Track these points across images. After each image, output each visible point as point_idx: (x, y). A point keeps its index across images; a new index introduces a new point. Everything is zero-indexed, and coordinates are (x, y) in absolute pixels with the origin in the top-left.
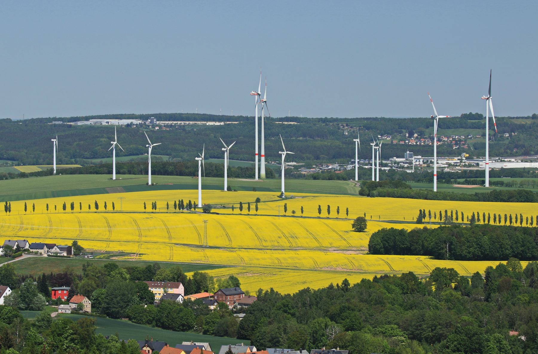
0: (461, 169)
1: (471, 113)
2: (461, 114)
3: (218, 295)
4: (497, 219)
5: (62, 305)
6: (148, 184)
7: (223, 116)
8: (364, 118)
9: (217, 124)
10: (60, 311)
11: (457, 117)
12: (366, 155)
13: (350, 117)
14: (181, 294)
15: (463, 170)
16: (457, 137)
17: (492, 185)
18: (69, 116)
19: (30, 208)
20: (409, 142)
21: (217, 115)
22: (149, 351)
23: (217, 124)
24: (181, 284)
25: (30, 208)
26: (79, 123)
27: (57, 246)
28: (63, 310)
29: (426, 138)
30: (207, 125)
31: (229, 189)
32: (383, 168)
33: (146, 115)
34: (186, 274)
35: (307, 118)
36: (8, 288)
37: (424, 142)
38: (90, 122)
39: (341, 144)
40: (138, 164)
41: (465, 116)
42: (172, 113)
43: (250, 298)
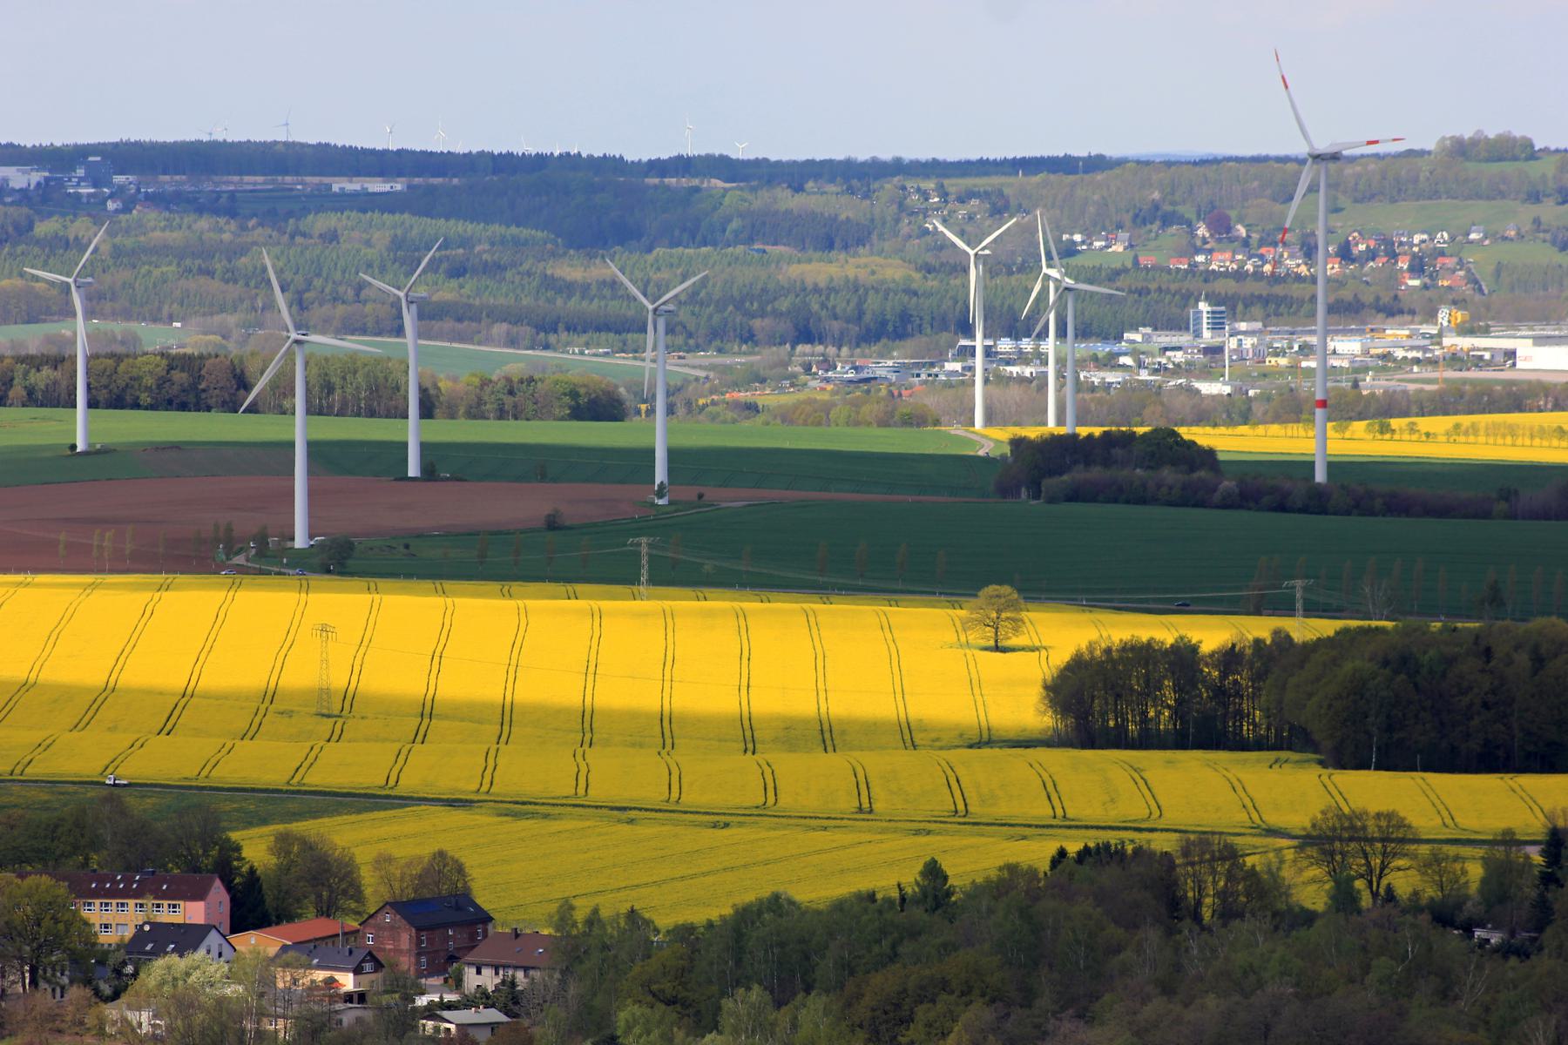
0: (1436, 375)
1: (225, 141)
3: (379, 928)
4: (522, 611)
6: (74, 447)
7: (400, 152)
8: (1014, 159)
14: (215, 927)
15: (1446, 380)
16: (1417, 239)
20: (1208, 262)
21: (379, 147)
24: (218, 883)
30: (335, 194)
33: (151, 142)
34: (235, 836)
35: (766, 160)
37: (1277, 263)
39: (917, 276)
40: (35, 362)
41: (1461, 150)
42: (46, 142)
43: (519, 939)
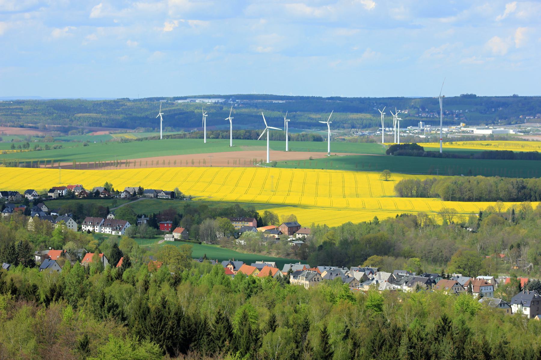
2: (513, 94)
5: (167, 235)
9: (281, 102)
10: (166, 239)
11: (458, 97)
12: (389, 125)
13: (378, 97)
17: (145, 117)
18: (172, 96)
19: (439, 279)
22: (231, 268)
23: (281, 102)
25: (439, 279)
26: (274, 101)
27: (164, 191)
28: (168, 238)
29: (434, 112)
31: (290, 150)
32: (402, 135)
34: (258, 211)
36: (128, 222)
38: (187, 101)
